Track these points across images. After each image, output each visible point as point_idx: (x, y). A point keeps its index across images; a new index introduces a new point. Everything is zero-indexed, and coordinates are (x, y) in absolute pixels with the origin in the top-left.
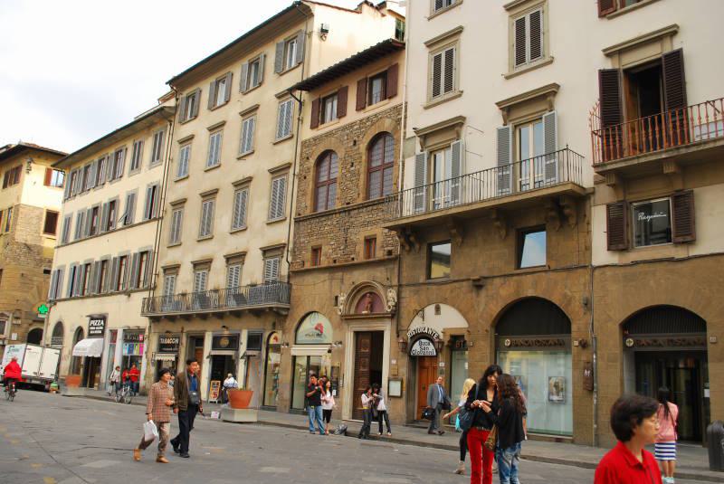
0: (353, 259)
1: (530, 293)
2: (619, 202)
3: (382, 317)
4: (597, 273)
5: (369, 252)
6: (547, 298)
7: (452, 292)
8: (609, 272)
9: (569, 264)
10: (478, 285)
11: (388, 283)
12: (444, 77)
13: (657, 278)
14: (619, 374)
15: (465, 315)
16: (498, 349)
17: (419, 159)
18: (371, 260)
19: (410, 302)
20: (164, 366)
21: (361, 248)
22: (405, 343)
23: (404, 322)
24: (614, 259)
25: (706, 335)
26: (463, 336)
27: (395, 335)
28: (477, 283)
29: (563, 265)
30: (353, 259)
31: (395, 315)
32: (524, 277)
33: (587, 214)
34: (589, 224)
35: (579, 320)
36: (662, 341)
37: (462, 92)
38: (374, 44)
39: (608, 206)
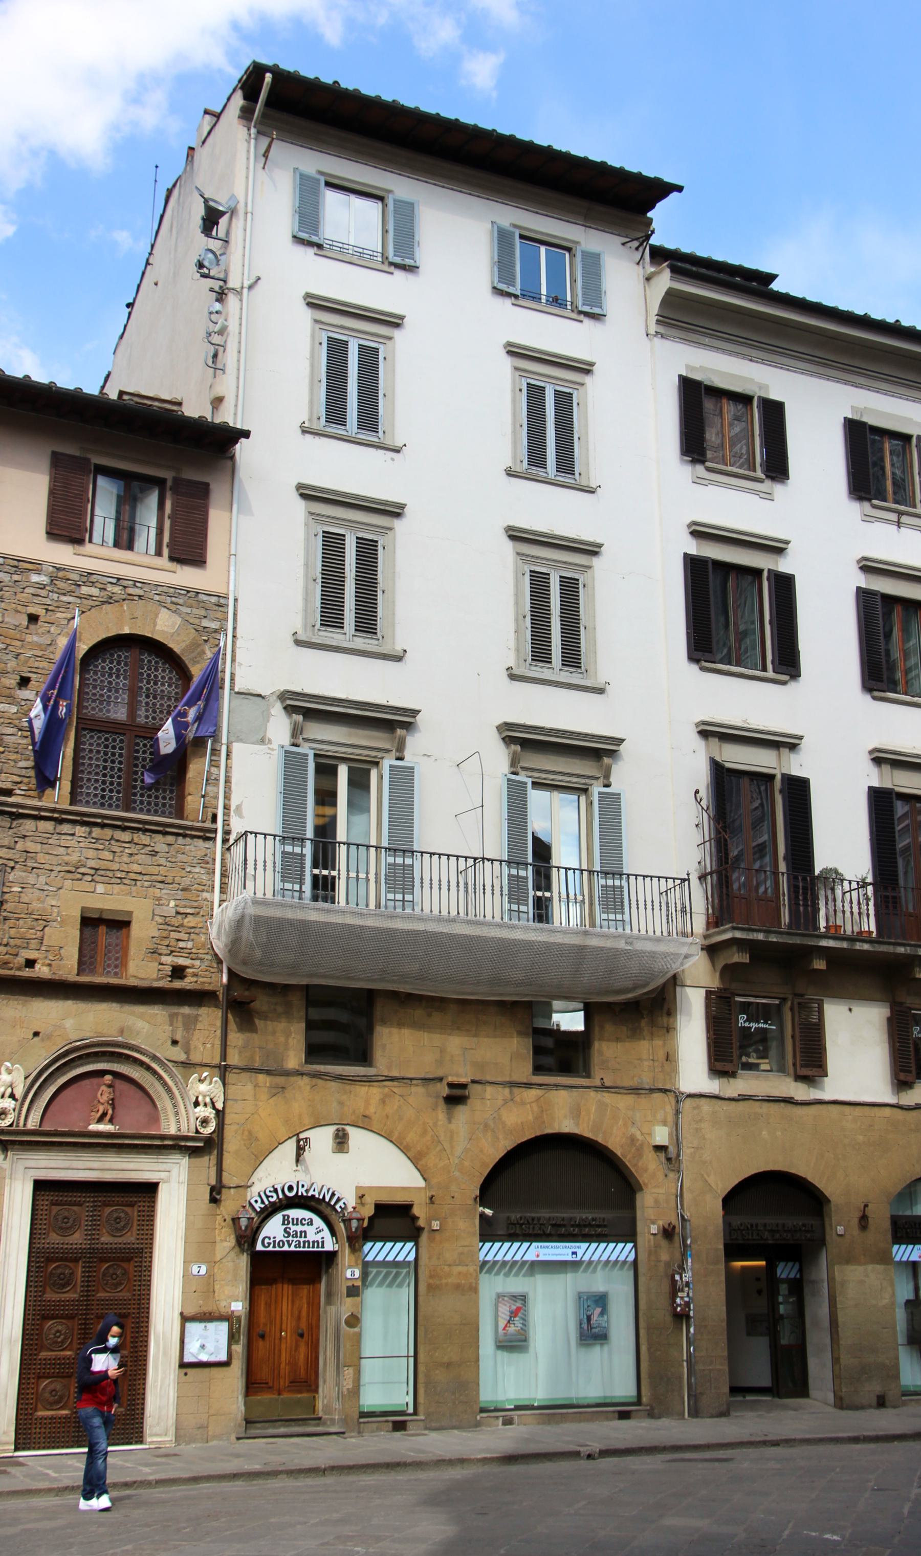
0: (30, 963)
1: (567, 1126)
7: (383, 1102)
10: (456, 1097)
12: (350, 585)
15: (416, 1160)
20: (223, 622)
24: (712, 1086)
29: (627, 1083)
30: (30, 963)
35: (657, 1187)
36: (769, 1222)
38: (387, 97)
39: (709, 993)
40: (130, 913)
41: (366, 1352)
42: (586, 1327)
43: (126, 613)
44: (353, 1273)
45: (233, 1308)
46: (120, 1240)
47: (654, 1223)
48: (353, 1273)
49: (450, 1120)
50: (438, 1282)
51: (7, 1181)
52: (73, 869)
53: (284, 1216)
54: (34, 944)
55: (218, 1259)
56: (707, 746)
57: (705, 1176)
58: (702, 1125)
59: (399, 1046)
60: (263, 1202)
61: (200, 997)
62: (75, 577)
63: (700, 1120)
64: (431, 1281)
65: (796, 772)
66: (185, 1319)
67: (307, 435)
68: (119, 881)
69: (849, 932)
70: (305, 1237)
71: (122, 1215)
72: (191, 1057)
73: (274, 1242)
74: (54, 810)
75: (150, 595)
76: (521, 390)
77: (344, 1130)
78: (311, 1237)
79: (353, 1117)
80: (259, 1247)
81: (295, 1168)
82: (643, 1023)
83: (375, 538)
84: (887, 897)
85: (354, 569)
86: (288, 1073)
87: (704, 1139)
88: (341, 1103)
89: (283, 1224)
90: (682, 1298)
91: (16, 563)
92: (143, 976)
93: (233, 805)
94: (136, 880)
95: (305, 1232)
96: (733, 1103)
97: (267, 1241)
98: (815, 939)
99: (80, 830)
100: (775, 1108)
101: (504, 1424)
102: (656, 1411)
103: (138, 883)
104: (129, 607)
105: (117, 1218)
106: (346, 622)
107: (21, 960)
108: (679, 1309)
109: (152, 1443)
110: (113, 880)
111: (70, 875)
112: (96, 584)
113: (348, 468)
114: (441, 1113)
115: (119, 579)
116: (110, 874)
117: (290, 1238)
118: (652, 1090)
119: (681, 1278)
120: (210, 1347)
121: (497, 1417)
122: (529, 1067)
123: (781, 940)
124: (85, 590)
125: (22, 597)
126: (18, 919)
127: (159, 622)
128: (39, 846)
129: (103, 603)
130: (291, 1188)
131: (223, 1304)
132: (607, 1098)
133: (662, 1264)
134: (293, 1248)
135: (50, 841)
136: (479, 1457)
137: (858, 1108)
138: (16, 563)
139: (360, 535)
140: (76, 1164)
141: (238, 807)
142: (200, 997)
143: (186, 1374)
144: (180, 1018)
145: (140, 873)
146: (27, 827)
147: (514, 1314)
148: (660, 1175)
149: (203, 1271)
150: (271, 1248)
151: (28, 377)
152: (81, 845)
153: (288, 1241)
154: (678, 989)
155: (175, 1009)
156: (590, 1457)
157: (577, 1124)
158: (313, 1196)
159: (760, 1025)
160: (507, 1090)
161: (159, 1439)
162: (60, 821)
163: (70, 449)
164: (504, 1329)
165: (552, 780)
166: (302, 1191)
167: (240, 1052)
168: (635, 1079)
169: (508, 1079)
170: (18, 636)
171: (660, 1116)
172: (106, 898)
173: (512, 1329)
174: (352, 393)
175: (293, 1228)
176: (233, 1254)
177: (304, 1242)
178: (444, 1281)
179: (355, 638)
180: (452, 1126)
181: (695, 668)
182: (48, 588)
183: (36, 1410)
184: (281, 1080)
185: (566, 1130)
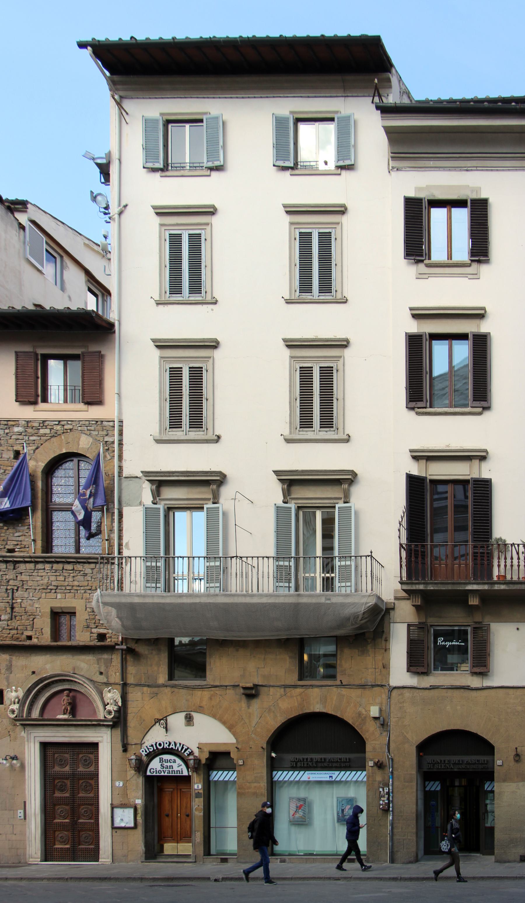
0: (30, 638)
1: (318, 708)
2: (420, 623)
3: (98, 724)
4: (395, 693)
5: (56, 633)
6: (339, 715)
7: (211, 699)
8: (407, 694)
9: (363, 682)
10: (251, 693)
11: (102, 679)
12: (187, 401)
13: (447, 701)
14: (415, 794)
15: (231, 728)
16: (273, 765)
17: (150, 515)
18: (59, 643)
19: (140, 703)
21: (44, 624)
22: (139, 760)
23: (133, 736)
24: (411, 680)
25: (494, 757)
26: (228, 754)
27: (119, 747)
28: (248, 692)
29: (357, 682)
31: (119, 721)
32: (310, 690)
33: (385, 630)
34: (387, 640)
37: (219, 437)
39: (409, 626)
40: (75, 608)
41: (211, 826)
42: (341, 815)
43: (64, 441)
44: (198, 786)
45: (136, 802)
46: (62, 770)
47: (371, 760)
48: (198, 786)
49: (249, 707)
50: (243, 791)
51: (26, 743)
52: (46, 587)
53: (160, 758)
54: (29, 628)
55: (129, 779)
56: (418, 466)
57: (405, 733)
58: (405, 705)
59: (221, 668)
60: (146, 751)
61: (111, 649)
62: (36, 424)
63: (403, 702)
64: (239, 791)
65: (485, 475)
66: (113, 808)
67: (160, 306)
68: (69, 591)
69: (515, 578)
70: (172, 768)
71: (88, 758)
72: (109, 680)
73: (156, 771)
74: (30, 557)
75: (76, 428)
76: (295, 239)
77: (190, 714)
78: (176, 768)
79: (194, 708)
80: (148, 773)
81: (166, 734)
82: (369, 647)
83: (200, 365)
84: (477, 553)
85: (188, 389)
86: (159, 686)
87: (406, 712)
88: (187, 700)
89: (160, 762)
90: (383, 801)
91: (6, 422)
92: (83, 640)
93: (124, 542)
94: (77, 590)
95: (172, 766)
96: (427, 690)
97: (152, 770)
98: (463, 585)
99: (48, 566)
100: (457, 693)
101: (281, 862)
102: (370, 859)
103: (79, 591)
104: (65, 438)
105: (85, 760)
106: (183, 423)
107: (24, 636)
108: (381, 807)
109: (101, 862)
110: (66, 591)
111: (44, 591)
112: (48, 427)
113: (186, 322)
114: (244, 703)
115: (59, 421)
116: (64, 588)
117: (164, 769)
118: (373, 686)
119: (383, 790)
120: (126, 819)
121: (277, 859)
122: (296, 676)
123: (436, 588)
124: (42, 431)
125: (11, 441)
126: (21, 616)
127: (81, 443)
128: (28, 577)
129: (52, 437)
130: (160, 745)
131: (132, 800)
132: (344, 691)
133: (377, 783)
134: (166, 774)
135: (33, 574)
136: (151, 877)
137: (519, 690)
138: (6, 422)
139: (191, 365)
140: (59, 734)
141: (127, 544)
142: (111, 649)
143: (116, 832)
144: (102, 660)
145: (79, 586)
146: (22, 568)
147: (299, 808)
148: (378, 732)
149: (121, 784)
150: (154, 774)
151: (68, 308)
152: (49, 574)
153: (163, 771)
154: (391, 624)
155: (100, 656)
156: (216, 880)
157: (325, 707)
158: (172, 748)
159: (453, 643)
160: (282, 690)
161: (104, 860)
162: (37, 563)
163: (27, 348)
164: (293, 815)
165: (312, 503)
166: (166, 746)
167: (134, 676)
168: (363, 680)
169: (283, 684)
170: (9, 464)
171: (378, 700)
172: (61, 601)
173: (297, 815)
174: (186, 270)
175: (166, 764)
176: (135, 777)
177: (172, 771)
178: (247, 791)
179: (190, 433)
180: (250, 710)
181: (412, 414)
182: (23, 434)
183: (55, 845)
184: (155, 690)
185: (317, 710)
